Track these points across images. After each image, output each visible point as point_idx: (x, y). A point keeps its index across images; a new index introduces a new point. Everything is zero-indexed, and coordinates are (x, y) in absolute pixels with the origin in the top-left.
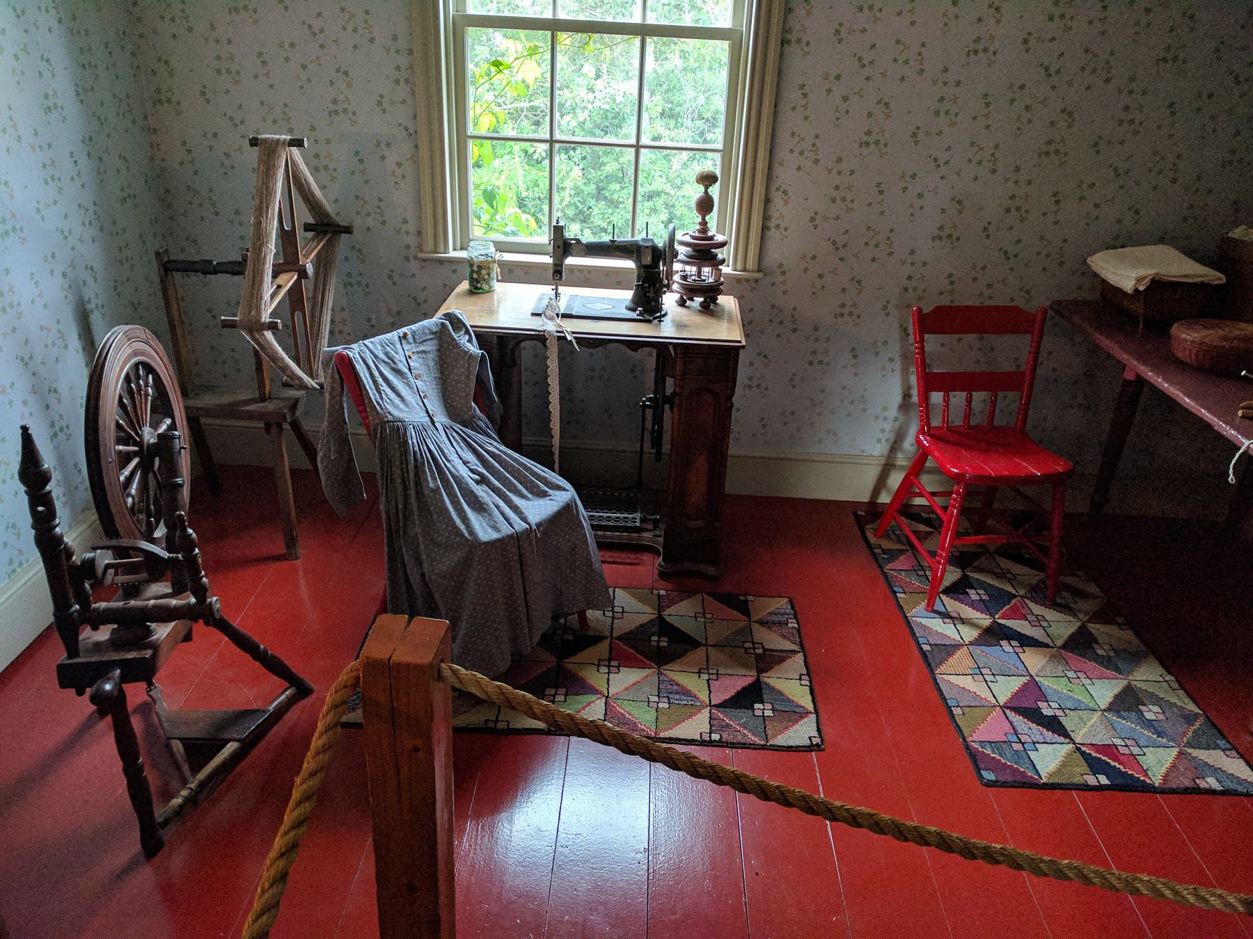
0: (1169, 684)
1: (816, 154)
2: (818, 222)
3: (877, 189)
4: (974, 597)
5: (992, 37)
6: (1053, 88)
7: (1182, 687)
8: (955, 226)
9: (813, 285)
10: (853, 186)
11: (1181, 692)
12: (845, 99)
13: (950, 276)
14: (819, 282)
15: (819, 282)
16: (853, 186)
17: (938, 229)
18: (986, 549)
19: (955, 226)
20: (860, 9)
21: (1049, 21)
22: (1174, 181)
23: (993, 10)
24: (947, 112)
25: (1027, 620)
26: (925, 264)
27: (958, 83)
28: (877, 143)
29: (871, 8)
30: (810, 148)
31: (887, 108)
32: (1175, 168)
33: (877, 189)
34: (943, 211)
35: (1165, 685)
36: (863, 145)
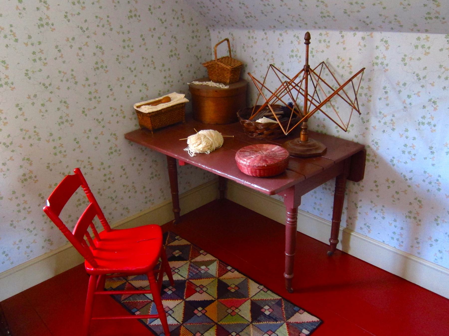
0: (263, 291)
1: (75, 79)
2: (86, 112)
3: (75, 142)
4: (170, 292)
5: (68, 115)
6: (103, 127)
7: (269, 289)
8: (116, 146)
9: (94, 144)
10: (62, 144)
11: (269, 292)
12: (80, 49)
13: (122, 167)
14: (96, 141)
15: (96, 141)
16: (62, 144)
17: (110, 149)
18: (175, 268)
19: (116, 146)
20: (74, 4)
21: (90, 101)
22: (136, 192)
23: (98, 49)
24: (128, 46)
25: (197, 292)
26: (109, 167)
27: (95, 84)
28: (102, 67)
29: (79, 2)
30: (71, 77)
31: (66, 104)
32: (134, 187)
33: (75, 142)
34: (109, 141)
35: (262, 292)
36: (61, 124)
